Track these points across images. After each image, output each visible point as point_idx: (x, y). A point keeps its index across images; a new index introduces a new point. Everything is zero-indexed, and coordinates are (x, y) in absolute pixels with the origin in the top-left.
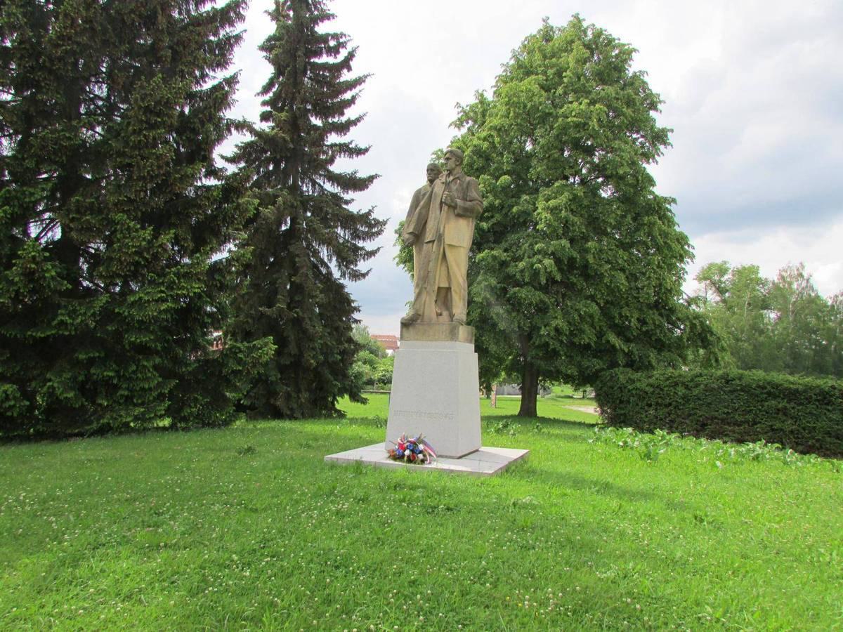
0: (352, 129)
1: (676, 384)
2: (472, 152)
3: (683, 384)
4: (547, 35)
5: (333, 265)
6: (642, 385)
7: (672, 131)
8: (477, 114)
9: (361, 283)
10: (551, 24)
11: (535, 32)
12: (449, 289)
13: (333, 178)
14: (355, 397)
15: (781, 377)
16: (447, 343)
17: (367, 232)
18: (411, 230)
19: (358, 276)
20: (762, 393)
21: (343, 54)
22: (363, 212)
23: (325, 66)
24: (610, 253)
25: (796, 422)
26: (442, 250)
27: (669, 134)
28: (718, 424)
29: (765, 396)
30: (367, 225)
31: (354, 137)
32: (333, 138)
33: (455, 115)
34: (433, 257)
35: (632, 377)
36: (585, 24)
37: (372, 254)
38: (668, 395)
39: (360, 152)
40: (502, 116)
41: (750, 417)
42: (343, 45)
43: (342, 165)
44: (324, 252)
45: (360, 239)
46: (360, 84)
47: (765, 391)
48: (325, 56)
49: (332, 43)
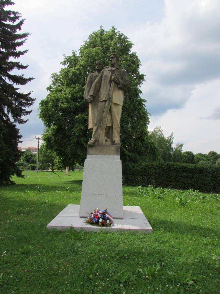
0: (21, 56)
1: (151, 168)
2: (72, 74)
3: (154, 168)
4: (102, 32)
5: (10, 116)
6: (138, 168)
7: (145, 75)
8: (72, 61)
9: (23, 125)
10: (103, 29)
11: (96, 31)
12: (112, 127)
13: (11, 77)
14: (19, 175)
15: (186, 165)
16: (114, 156)
17: (26, 103)
18: (92, 94)
19: (22, 122)
20: (181, 170)
21: (17, 22)
22: (25, 94)
23: (8, 26)
24: (126, 118)
25: (192, 180)
26: (110, 106)
27: (144, 77)
28: (166, 182)
29: (182, 171)
30: (27, 99)
31: (21, 60)
32: (12, 59)
33: (63, 60)
34: (106, 109)
35: (134, 165)
36: (116, 31)
37: (29, 113)
38: (148, 172)
39: (23, 67)
40: (85, 61)
41: (177, 179)
42: (17, 18)
43: (14, 72)
44: (6, 109)
45: (22, 106)
46: (25, 37)
47: (182, 170)
48: (8, 21)
49: (12, 16)
